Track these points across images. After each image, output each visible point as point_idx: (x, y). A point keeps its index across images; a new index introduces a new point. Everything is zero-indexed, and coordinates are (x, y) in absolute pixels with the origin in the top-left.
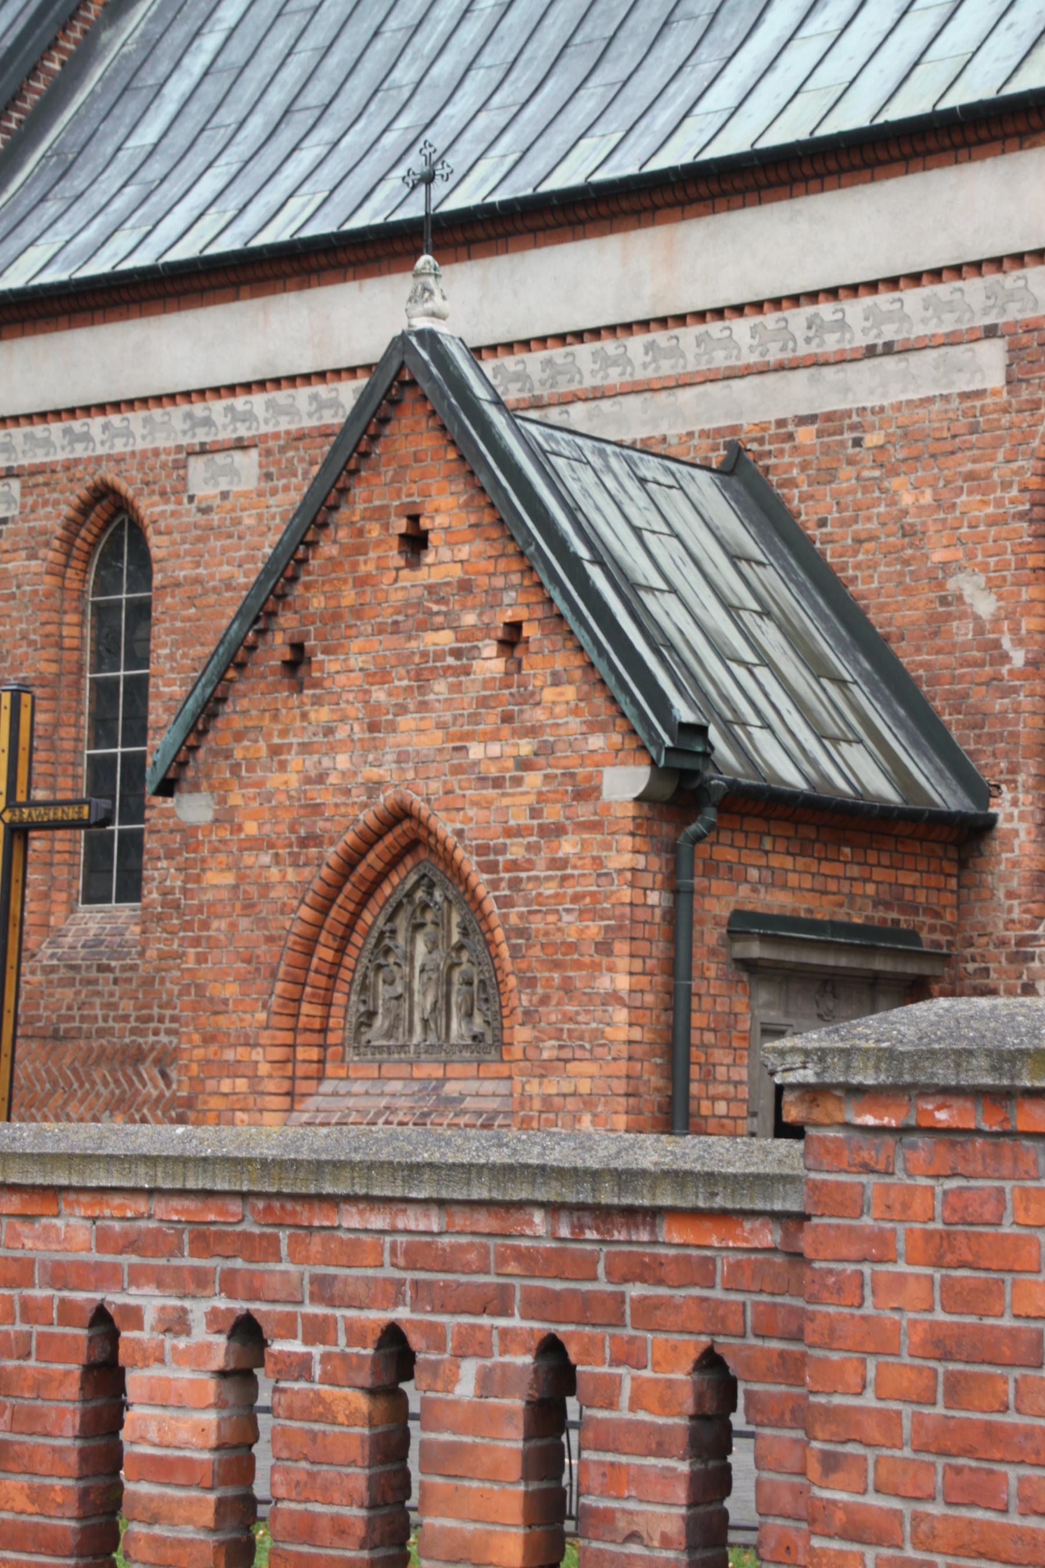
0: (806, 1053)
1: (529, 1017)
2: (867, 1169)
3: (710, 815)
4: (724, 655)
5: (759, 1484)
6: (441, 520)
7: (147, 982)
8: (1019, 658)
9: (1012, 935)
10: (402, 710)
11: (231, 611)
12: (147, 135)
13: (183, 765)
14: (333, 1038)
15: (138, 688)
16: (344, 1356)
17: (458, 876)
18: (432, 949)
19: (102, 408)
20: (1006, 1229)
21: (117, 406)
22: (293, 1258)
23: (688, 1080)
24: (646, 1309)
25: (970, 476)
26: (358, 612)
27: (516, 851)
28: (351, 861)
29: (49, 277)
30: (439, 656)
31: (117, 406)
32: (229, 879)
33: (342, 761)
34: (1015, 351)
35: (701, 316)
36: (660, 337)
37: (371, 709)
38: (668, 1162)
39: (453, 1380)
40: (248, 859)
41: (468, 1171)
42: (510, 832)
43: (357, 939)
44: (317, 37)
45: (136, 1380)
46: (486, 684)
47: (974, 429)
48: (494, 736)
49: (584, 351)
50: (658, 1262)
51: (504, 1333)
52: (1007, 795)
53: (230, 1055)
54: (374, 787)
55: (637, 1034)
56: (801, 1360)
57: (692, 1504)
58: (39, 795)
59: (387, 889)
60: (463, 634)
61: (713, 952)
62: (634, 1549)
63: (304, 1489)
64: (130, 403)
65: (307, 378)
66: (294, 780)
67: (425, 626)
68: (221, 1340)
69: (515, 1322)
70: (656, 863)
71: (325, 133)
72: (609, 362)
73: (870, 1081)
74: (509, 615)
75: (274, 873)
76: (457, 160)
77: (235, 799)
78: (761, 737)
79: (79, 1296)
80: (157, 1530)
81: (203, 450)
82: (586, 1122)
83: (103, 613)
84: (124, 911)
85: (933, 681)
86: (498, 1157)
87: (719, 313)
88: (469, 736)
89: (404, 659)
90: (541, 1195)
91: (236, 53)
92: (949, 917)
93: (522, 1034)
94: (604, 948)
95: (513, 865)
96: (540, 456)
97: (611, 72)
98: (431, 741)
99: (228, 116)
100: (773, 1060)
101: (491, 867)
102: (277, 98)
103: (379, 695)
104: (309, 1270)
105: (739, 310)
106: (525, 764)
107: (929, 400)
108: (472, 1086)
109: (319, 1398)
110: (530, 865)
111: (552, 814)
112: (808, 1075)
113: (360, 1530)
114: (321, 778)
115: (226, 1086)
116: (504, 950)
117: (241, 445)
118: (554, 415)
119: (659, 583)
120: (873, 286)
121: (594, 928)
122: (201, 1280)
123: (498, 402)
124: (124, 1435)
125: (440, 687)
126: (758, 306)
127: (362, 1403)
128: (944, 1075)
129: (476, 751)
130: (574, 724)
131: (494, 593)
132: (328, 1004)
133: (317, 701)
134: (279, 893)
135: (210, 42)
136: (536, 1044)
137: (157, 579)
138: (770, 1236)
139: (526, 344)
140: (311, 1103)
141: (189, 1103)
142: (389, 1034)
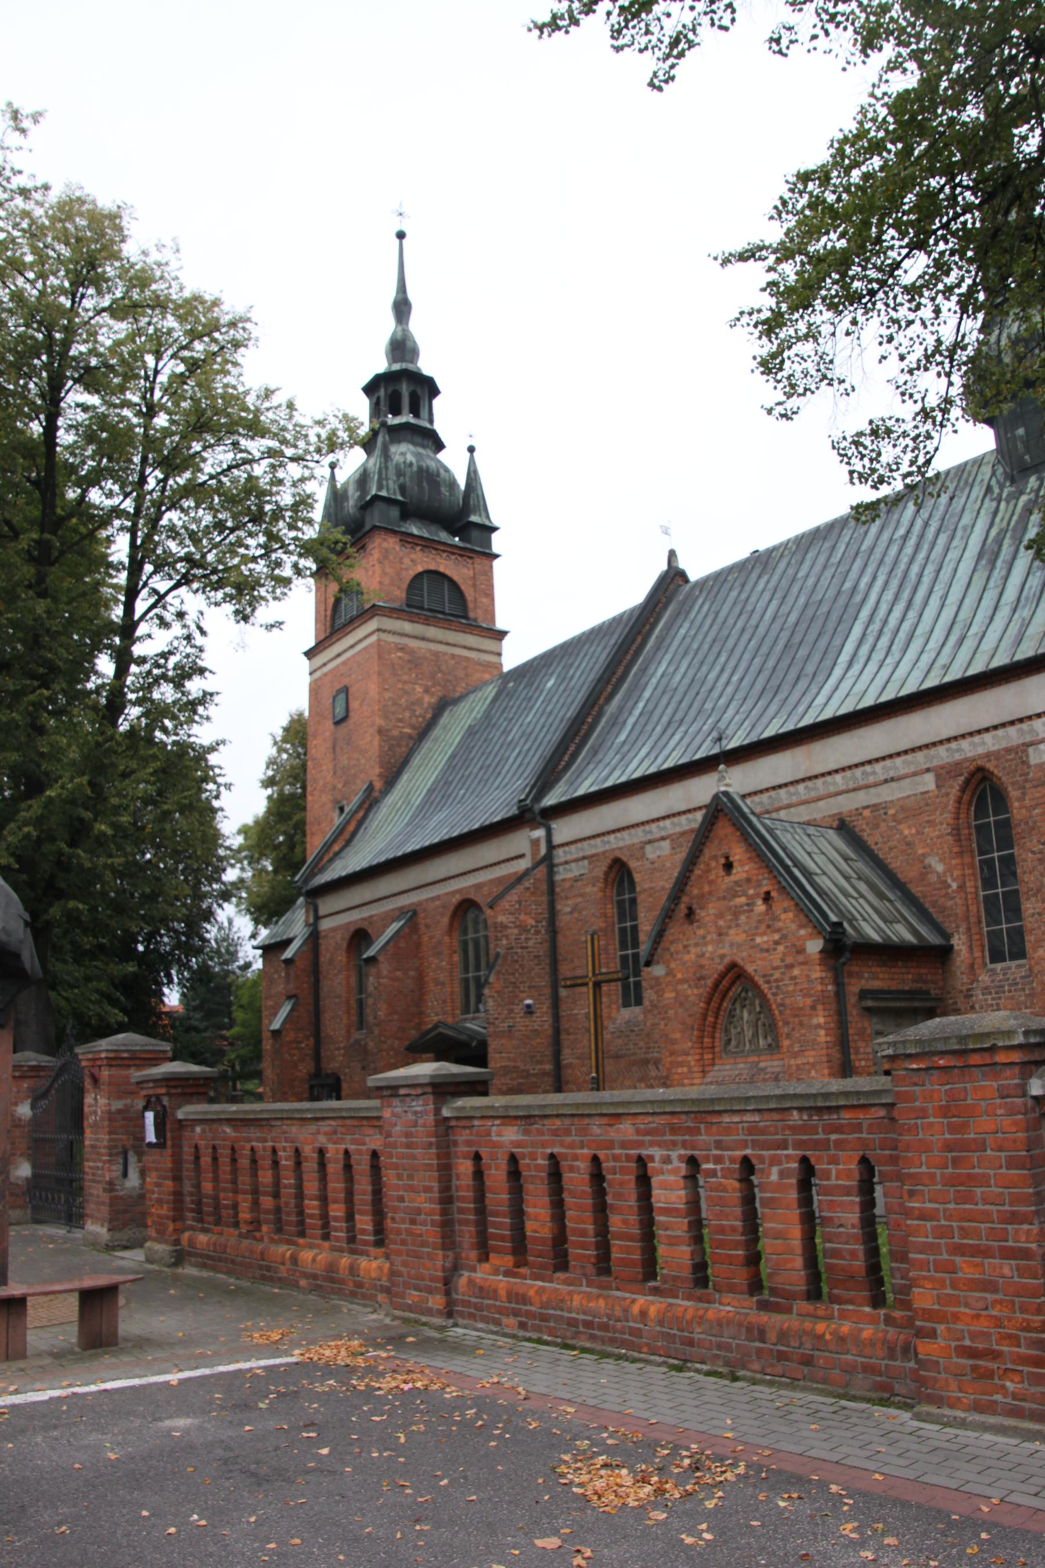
0: (889, 1043)
1: (788, 1036)
2: (915, 1084)
3: (847, 955)
4: (846, 895)
5: (886, 1204)
6: (737, 857)
7: (648, 1035)
8: (954, 885)
9: (964, 988)
10: (730, 927)
11: (665, 898)
12: (622, 737)
14: (717, 1050)
15: (635, 929)
16: (729, 1169)
17: (756, 986)
18: (750, 1013)
19: (613, 832)
20: (969, 1101)
21: (619, 830)
22: (707, 1134)
23: (849, 1054)
24: (839, 1144)
25: (928, 822)
26: (710, 893)
27: (777, 975)
28: (717, 984)
29: (592, 789)
31: (619, 830)
32: (673, 995)
33: (710, 948)
34: (938, 776)
35: (823, 775)
36: (809, 784)
37: (719, 928)
38: (841, 1089)
39: (769, 1175)
40: (680, 987)
41: (768, 1098)
42: (774, 968)
44: (677, 698)
45: (655, 1181)
46: (760, 915)
47: (927, 805)
48: (764, 934)
49: (782, 792)
50: (841, 1126)
51: (787, 1156)
52: (956, 936)
53: (680, 1059)
54: (722, 957)
55: (829, 1039)
56: (897, 1157)
57: (862, 1212)
58: (604, 970)
59: (731, 994)
60: (749, 897)
61: (854, 1006)
62: (841, 1230)
63: (719, 1216)
65: (684, 812)
66: (693, 956)
67: (736, 895)
68: (683, 1165)
69: (790, 1152)
70: (830, 975)
71: (683, 729)
72: (791, 794)
73: (913, 1052)
74: (765, 889)
75: (689, 992)
76: (729, 732)
77: (673, 965)
78: (863, 924)
79: (632, 1152)
80: (668, 1233)
81: (650, 842)
82: (813, 1073)
83: (620, 903)
84: (637, 1010)
85: (925, 897)
86: (778, 1092)
87: (829, 773)
89: (729, 909)
90: (795, 1105)
91: (650, 707)
92: (940, 984)
93: (786, 1043)
94: (813, 1008)
95: (777, 981)
96: (770, 831)
97: (781, 696)
98: (741, 938)
99: (649, 728)
100: (876, 1048)
101: (768, 982)
102: (665, 719)
103: (721, 923)
104: (712, 1138)
105: (836, 771)
106: (777, 943)
107: (909, 796)
108: (769, 1063)
109: (721, 1184)
110: (782, 980)
111: (789, 960)
112: (890, 1052)
113: (741, 1229)
114: (703, 955)
115: (680, 1070)
116: (776, 1012)
117: (663, 839)
118: (774, 815)
119: (818, 871)
120: (883, 758)
121: (809, 1001)
122: (674, 1145)
123: (753, 813)
124: (653, 1200)
125: (743, 918)
126: (843, 769)
127: (737, 1185)
128: (941, 1047)
129: (758, 940)
130: (794, 926)
131: (759, 882)
132: (713, 1037)
133: (699, 927)
134: (692, 998)
135: (641, 705)
136: (791, 1046)
137: (638, 889)
138: (882, 1113)
139: (761, 792)
140: (711, 1074)
141: (667, 1077)
142: (737, 1047)
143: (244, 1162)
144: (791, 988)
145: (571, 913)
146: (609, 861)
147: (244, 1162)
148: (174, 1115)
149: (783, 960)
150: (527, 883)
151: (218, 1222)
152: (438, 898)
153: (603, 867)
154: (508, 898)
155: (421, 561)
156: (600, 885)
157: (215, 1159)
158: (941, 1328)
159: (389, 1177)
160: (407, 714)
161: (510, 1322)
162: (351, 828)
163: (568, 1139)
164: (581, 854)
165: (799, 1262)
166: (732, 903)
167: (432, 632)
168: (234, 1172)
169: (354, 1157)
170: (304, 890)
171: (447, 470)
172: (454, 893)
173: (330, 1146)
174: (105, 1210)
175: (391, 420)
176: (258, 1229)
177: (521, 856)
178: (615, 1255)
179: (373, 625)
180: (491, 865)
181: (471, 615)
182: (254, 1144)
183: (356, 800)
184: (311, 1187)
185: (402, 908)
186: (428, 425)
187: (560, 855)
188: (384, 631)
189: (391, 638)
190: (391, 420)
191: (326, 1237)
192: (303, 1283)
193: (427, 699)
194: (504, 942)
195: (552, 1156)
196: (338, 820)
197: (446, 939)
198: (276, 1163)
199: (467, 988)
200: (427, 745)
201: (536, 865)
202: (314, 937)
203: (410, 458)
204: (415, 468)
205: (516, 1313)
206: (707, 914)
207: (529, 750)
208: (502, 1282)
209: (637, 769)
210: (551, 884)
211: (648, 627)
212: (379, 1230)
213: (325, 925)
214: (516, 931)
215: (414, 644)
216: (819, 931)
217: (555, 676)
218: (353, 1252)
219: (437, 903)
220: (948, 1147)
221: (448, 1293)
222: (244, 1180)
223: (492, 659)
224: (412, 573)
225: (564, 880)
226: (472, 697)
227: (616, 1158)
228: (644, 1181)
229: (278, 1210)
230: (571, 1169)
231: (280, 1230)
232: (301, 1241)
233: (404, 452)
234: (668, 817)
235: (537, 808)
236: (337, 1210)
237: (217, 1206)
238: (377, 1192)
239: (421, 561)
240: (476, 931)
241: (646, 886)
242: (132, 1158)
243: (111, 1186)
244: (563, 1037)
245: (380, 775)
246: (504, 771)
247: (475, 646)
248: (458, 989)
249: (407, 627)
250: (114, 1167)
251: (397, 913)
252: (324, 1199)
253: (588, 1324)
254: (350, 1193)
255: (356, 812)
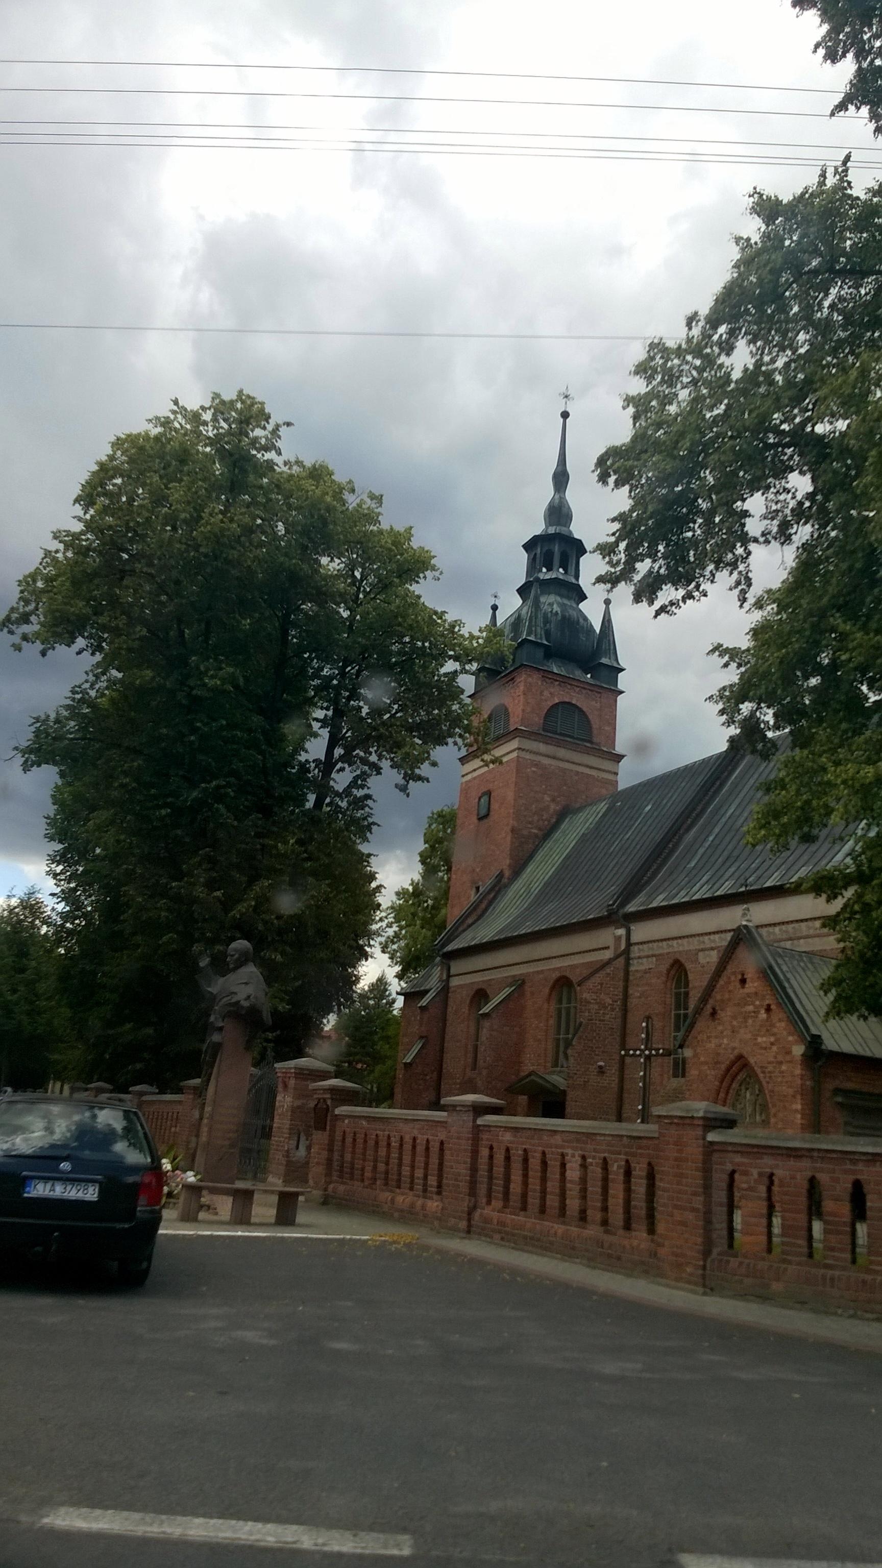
1: (775, 1115)
10: (740, 1027)
12: (693, 864)
13: (685, 1041)
18: (751, 1095)
21: (680, 938)
26: (729, 1000)
27: (770, 1068)
28: (728, 1070)
30: (750, 1012)
32: (696, 1072)
33: (725, 1041)
43: (731, 1091)
45: (568, 1166)
49: (803, 925)
54: (734, 1049)
55: (803, 1122)
60: (756, 1007)
64: (684, 937)
66: (713, 1045)
67: (746, 1004)
71: (737, 864)
74: (767, 1002)
75: (708, 1072)
81: (702, 950)
83: (678, 995)
88: (758, 1035)
91: (716, 842)
93: (773, 1120)
94: (794, 1096)
95: (770, 1072)
98: (749, 1036)
99: (713, 859)
101: (763, 1072)
102: (726, 853)
103: (735, 1023)
110: (774, 1072)
111: (780, 1058)
117: (712, 949)
125: (750, 1021)
129: (760, 1040)
130: (785, 1033)
133: (719, 1024)
137: (690, 986)
139: (787, 923)
143: (371, 1143)
144: (779, 1079)
145: (640, 997)
146: (671, 961)
147: (371, 1143)
148: (333, 1111)
149: (775, 1057)
150: (608, 970)
151: (352, 1179)
152: (542, 972)
153: (664, 968)
154: (593, 980)
155: (556, 695)
156: (664, 979)
157: (354, 1140)
158: (667, 1243)
159: (448, 1155)
160: (536, 818)
161: (497, 1236)
162: (483, 906)
163: (533, 1142)
164: (651, 953)
165: (621, 1211)
166: (743, 1010)
167: (562, 752)
168: (365, 1149)
169: (431, 1143)
170: (441, 953)
171: (586, 619)
172: (554, 970)
173: (420, 1136)
174: (282, 1168)
175: (544, 574)
176: (374, 1183)
177: (607, 948)
178: (548, 1203)
179: (514, 744)
180: (584, 952)
181: (595, 740)
182: (378, 1132)
183: (489, 882)
184: (407, 1159)
185: (514, 976)
186: (574, 581)
187: (635, 951)
188: (523, 750)
189: (528, 756)
190: (544, 574)
191: (411, 1189)
192: (396, 1215)
193: (553, 807)
194: (587, 1014)
195: (525, 1150)
196: (473, 897)
197: (546, 1006)
198: (389, 1145)
199: (558, 1046)
200: (549, 844)
201: (617, 957)
202: (445, 990)
203: (556, 608)
204: (559, 618)
205: (500, 1232)
206: (725, 1015)
207: (625, 861)
208: (495, 1215)
209: (701, 892)
210: (627, 973)
211: (726, 774)
212: (439, 1186)
213: (455, 982)
214: (596, 1007)
215: (546, 761)
216: (802, 1038)
217: (652, 802)
218: (425, 1197)
219: (541, 976)
220: (676, 1159)
221: (469, 1220)
222: (370, 1153)
223: (611, 777)
224: (550, 704)
225: (637, 971)
226: (588, 809)
227: (552, 1153)
228: (563, 1165)
229: (387, 1173)
230: (533, 1157)
231: (386, 1184)
232: (398, 1190)
233: (552, 602)
234: (717, 932)
235: (621, 912)
236: (419, 1173)
237: (352, 1168)
238: (441, 1164)
239: (556, 695)
240: (569, 1002)
241: (697, 984)
242: (303, 1138)
243: (287, 1154)
244: (625, 1095)
245: (510, 866)
246: (603, 877)
247: (595, 765)
248: (550, 1046)
249: (542, 747)
250: (291, 1142)
251: (510, 980)
252: (413, 1167)
253: (532, 1238)
254: (427, 1164)
255: (489, 892)
